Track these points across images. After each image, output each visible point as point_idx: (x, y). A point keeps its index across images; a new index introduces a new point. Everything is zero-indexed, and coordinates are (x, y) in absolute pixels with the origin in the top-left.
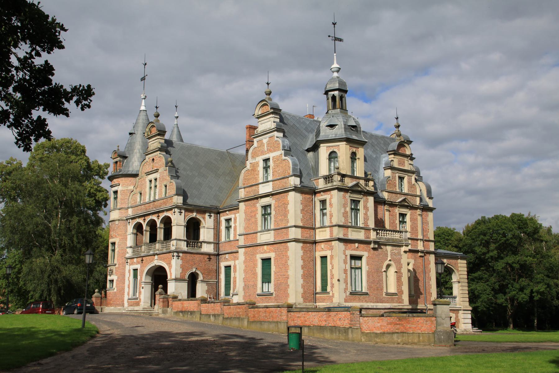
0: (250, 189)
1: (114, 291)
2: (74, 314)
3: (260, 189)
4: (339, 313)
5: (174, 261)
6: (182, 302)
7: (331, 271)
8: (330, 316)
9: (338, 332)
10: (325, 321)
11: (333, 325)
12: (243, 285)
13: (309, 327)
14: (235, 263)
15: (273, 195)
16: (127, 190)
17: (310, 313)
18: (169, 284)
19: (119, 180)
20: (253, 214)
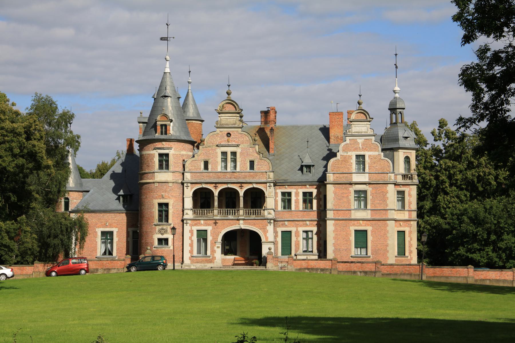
0: (341, 175)
1: (170, 249)
2: (157, 270)
3: (138, 137)
4: (507, 272)
5: (270, 228)
6: (306, 261)
7: (410, 242)
8: (502, 274)
9: (507, 283)
10: (500, 276)
11: (504, 279)
12: (333, 248)
13: (489, 280)
14: (297, 230)
15: (369, 184)
16: (180, 154)
17: (490, 272)
18: (263, 246)
19: (171, 144)
20: (345, 195)
